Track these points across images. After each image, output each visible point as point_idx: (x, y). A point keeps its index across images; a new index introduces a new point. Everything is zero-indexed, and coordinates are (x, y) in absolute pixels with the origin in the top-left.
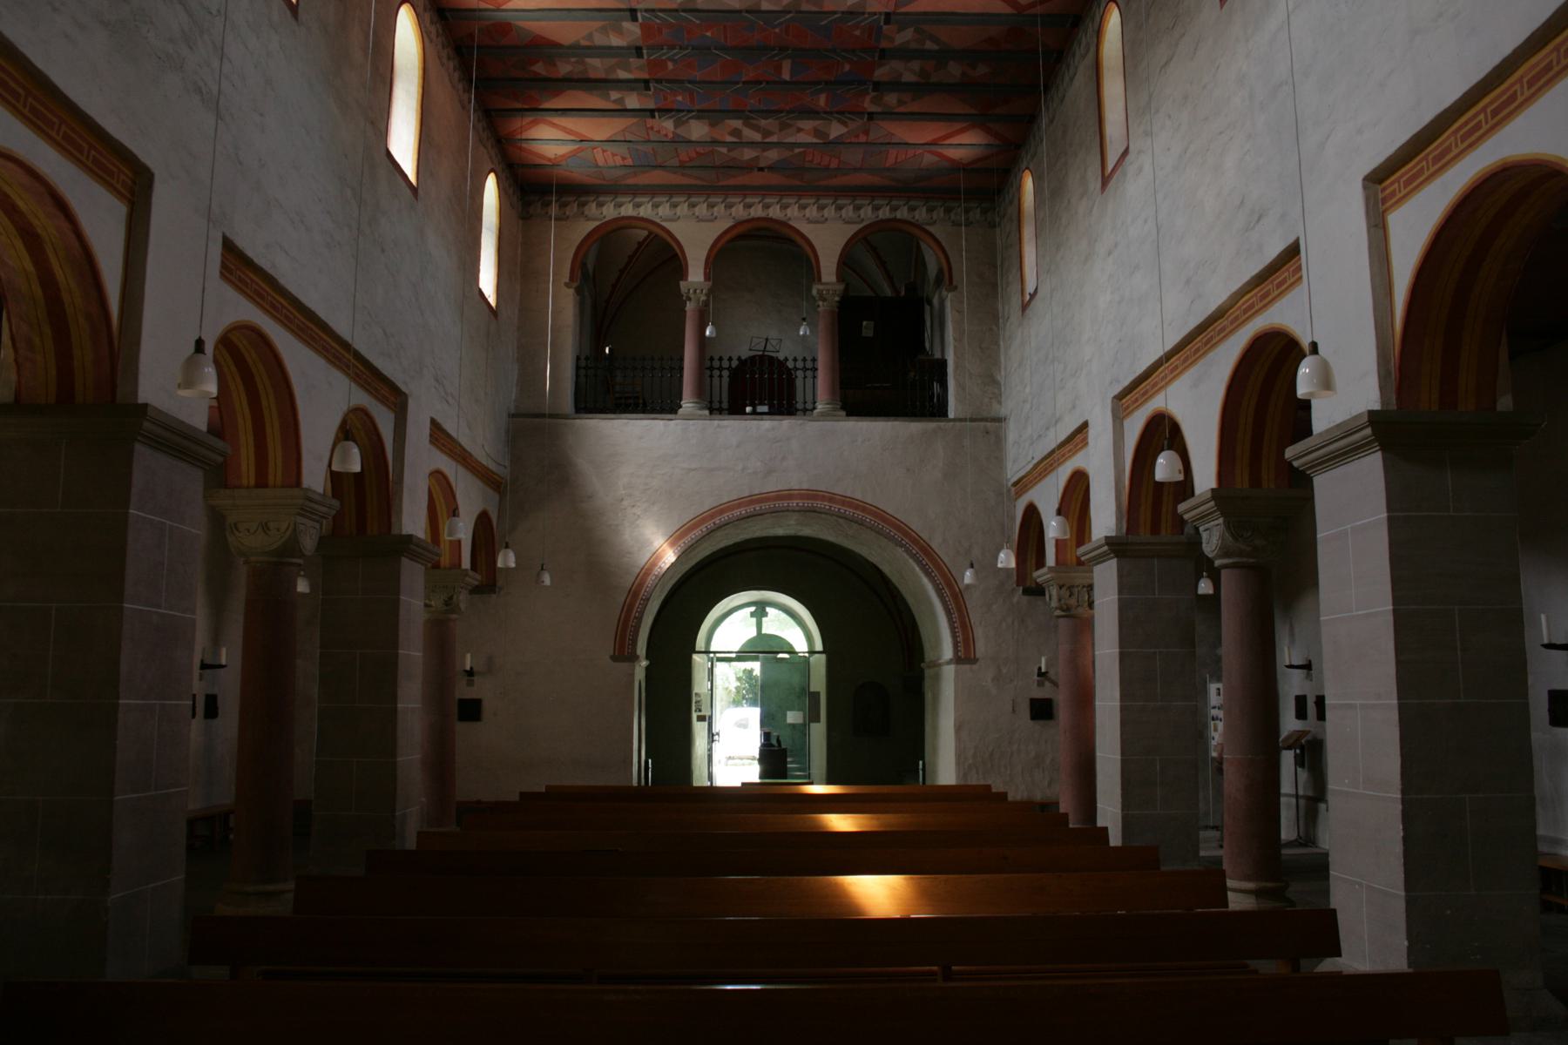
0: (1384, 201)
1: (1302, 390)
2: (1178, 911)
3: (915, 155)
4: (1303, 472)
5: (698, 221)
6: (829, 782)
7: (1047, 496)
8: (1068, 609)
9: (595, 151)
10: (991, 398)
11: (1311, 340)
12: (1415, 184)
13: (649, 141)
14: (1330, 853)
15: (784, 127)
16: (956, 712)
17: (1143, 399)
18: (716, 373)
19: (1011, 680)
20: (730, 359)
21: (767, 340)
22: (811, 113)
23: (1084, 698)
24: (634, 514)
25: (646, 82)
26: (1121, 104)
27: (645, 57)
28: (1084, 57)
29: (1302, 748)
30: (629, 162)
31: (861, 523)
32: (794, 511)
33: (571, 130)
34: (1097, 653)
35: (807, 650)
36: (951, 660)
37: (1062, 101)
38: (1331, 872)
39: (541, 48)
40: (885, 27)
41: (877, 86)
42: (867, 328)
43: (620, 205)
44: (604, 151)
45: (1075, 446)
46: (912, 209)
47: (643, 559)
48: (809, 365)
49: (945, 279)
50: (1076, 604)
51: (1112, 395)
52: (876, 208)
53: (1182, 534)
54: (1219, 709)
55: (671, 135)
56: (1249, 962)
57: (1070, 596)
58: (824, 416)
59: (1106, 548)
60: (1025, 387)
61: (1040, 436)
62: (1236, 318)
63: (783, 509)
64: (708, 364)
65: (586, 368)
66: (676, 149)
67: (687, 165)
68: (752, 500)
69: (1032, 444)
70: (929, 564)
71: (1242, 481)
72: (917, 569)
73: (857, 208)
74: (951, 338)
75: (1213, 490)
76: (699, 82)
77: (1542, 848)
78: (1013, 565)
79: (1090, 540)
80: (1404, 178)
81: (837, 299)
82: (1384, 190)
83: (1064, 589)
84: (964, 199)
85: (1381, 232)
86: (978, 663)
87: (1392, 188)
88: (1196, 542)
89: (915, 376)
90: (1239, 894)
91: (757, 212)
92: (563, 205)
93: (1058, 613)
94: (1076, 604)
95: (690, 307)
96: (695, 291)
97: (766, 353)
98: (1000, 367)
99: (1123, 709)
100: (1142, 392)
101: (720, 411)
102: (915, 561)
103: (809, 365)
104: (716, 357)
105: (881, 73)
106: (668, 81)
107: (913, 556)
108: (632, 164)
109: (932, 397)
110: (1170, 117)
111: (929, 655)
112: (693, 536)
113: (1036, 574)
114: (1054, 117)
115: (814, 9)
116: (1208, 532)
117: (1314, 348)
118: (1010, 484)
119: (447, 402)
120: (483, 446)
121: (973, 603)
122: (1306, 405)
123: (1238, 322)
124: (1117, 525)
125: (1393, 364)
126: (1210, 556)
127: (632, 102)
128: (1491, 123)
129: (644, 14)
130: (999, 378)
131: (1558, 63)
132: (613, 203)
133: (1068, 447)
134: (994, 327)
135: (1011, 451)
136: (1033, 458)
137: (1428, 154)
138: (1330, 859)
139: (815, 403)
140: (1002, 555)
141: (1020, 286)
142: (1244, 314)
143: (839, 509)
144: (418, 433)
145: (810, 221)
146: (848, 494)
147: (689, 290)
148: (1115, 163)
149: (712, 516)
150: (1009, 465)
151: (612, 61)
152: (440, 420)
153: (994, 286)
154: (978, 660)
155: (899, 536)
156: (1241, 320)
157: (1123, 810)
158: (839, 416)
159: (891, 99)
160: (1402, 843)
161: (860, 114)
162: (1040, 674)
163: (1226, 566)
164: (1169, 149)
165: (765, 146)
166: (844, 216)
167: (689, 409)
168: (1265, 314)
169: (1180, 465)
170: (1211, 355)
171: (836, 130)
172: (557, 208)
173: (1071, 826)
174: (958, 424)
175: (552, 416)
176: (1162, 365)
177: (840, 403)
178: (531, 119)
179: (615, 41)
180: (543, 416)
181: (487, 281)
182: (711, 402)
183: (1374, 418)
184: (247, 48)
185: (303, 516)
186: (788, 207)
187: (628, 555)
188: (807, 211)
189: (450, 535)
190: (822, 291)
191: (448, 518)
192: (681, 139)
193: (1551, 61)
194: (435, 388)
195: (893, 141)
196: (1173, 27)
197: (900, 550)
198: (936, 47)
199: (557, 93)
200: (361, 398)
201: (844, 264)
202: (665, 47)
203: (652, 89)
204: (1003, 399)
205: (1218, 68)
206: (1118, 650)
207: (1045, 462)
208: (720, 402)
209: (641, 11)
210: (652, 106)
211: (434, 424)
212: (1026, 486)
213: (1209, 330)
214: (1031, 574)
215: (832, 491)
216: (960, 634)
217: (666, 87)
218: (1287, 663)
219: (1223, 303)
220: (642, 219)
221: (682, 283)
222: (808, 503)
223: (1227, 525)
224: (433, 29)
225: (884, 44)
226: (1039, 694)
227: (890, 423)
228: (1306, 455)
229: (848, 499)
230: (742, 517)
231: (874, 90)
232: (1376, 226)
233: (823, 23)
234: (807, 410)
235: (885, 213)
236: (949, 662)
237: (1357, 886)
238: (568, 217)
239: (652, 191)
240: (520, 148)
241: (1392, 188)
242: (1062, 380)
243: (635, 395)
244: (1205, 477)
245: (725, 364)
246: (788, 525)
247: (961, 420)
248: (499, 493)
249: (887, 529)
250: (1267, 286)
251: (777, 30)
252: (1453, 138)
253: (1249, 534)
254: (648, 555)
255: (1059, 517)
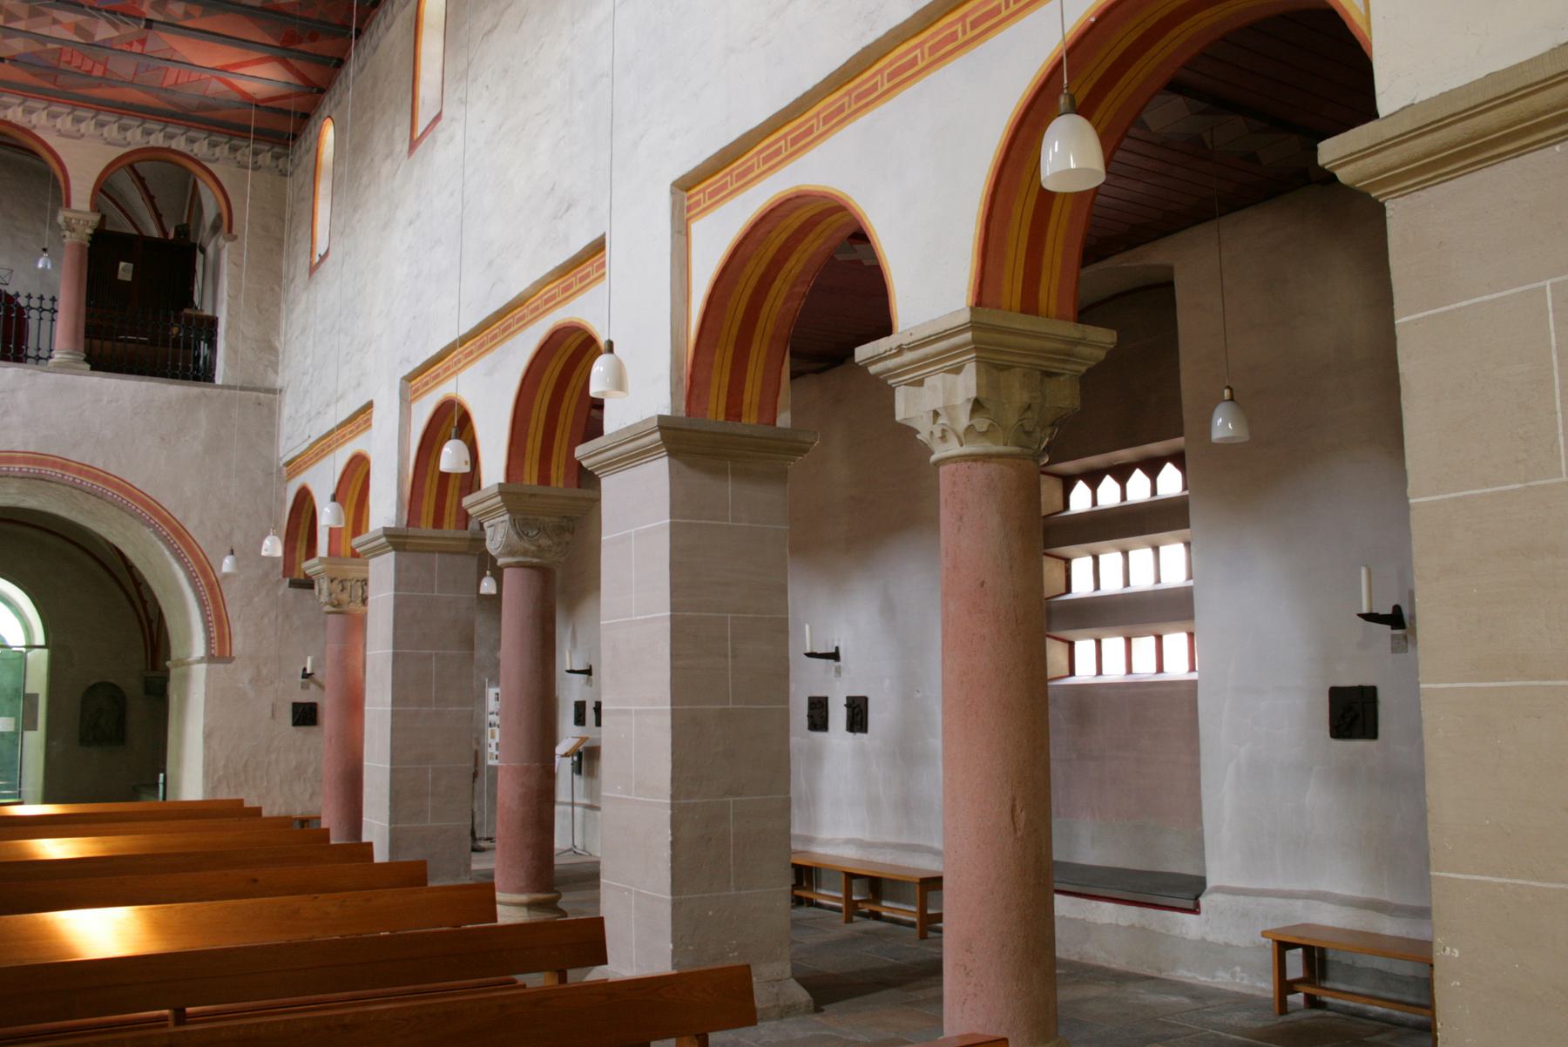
0: (689, 209)
1: (595, 390)
2: (445, 929)
3: (200, 80)
4: (591, 473)
5: (238, 167)
6: (47, 800)
7: (322, 480)
8: (339, 605)
10: (267, 366)
11: (607, 339)
12: (720, 196)
14: (602, 861)
16: (204, 718)
17: (434, 383)
19: (272, 682)
23: (353, 703)
26: (439, 65)
29: (580, 755)
34: (368, 653)
35: (24, 644)
36: (202, 658)
38: (602, 880)
42: (125, 271)
45: (358, 427)
48: (47, 304)
49: (224, 225)
50: (349, 599)
51: (401, 376)
53: (466, 529)
54: (497, 714)
56: (517, 977)
57: (342, 590)
58: (62, 368)
59: (384, 540)
60: (306, 358)
61: (319, 413)
62: (537, 308)
71: (530, 476)
72: (167, 553)
74: (225, 293)
75: (500, 484)
77: (795, 846)
78: (279, 552)
80: (709, 190)
81: (89, 231)
82: (689, 198)
83: (336, 582)
84: (254, 139)
85: (685, 238)
86: (234, 662)
87: (697, 198)
88: (479, 541)
89: (179, 332)
90: (512, 908)
93: (328, 608)
94: (349, 599)
98: (279, 332)
99: (394, 714)
100: (433, 375)
107: (164, 539)
111: (176, 652)
113: (305, 565)
116: (493, 528)
117: (610, 347)
118: (281, 463)
121: (231, 594)
122: (598, 405)
124: (397, 516)
125: (685, 371)
126: (493, 554)
128: (790, 150)
130: (277, 344)
131: (849, 107)
133: (350, 428)
134: (277, 288)
136: (309, 437)
137: (733, 170)
138: (601, 867)
140: (267, 542)
141: (309, 246)
142: (545, 304)
145: (60, 133)
153: (280, 242)
154: (234, 658)
155: (147, 514)
156: (541, 310)
157: (391, 823)
158: (83, 369)
160: (669, 847)
161: (137, 18)
162: (306, 676)
163: (509, 566)
164: (483, 122)
166: (106, 135)
169: (466, 456)
170: (508, 344)
171: (103, 31)
173: (333, 842)
174: (226, 392)
183: (666, 426)
188: (106, 130)
190: (71, 219)
193: (844, 104)
195: (174, 58)
197: (148, 531)
201: (102, 191)
205: (542, 46)
206: (391, 651)
212: (300, 466)
213: (508, 317)
214: (300, 564)
216: (214, 629)
218: (568, 669)
219: (524, 291)
222: (34, 469)
223: (513, 523)
226: (304, 697)
228: (595, 455)
229: (86, 468)
232: (679, 232)
234: (40, 358)
235: (157, 140)
236: (201, 661)
237: (626, 893)
241: (697, 198)
242: (348, 354)
244: (493, 471)
247: (229, 387)
249: (134, 505)
250: (571, 278)
252: (755, 159)
253: (535, 533)
255: (335, 504)
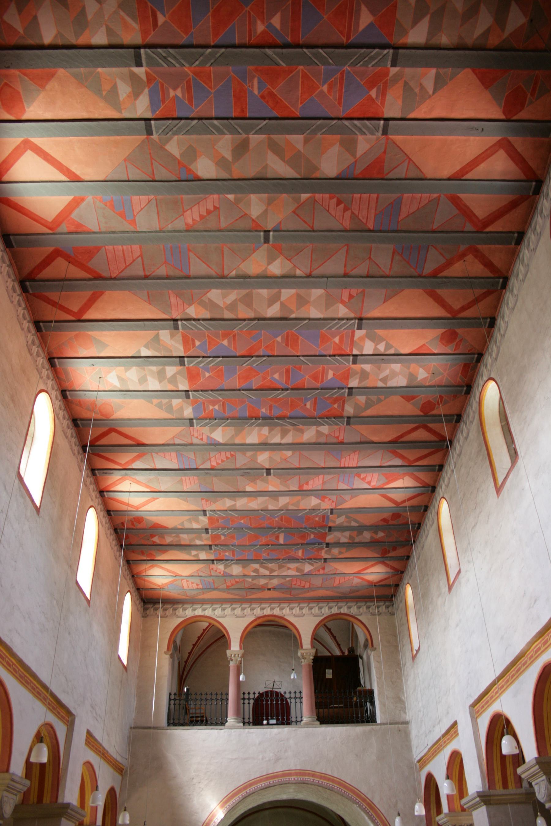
9: (183, 581)
13: (211, 576)
15: (281, 567)
18: (246, 701)
20: (254, 693)
21: (274, 682)
22: (295, 559)
24: (200, 787)
25: (210, 546)
27: (210, 533)
28: (432, 525)
30: (200, 587)
31: (331, 790)
32: (292, 783)
33: (171, 571)
37: (423, 548)
39: (157, 528)
40: (331, 516)
41: (328, 545)
42: (329, 674)
43: (194, 610)
44: (187, 581)
46: (349, 608)
47: (204, 817)
48: (298, 695)
49: (369, 644)
52: (330, 608)
53: (521, 787)
55: (222, 573)
58: (308, 725)
61: (430, 731)
62: (532, 656)
63: (286, 782)
64: (242, 696)
65: (175, 700)
66: (225, 580)
67: (230, 588)
68: (268, 777)
69: (426, 736)
70: (373, 814)
72: (367, 818)
73: (320, 608)
74: (375, 677)
75: (536, 758)
76: (238, 546)
78: (424, 813)
79: (467, 794)
88: (531, 794)
89: (357, 700)
91: (267, 612)
92: (165, 610)
95: (232, 664)
96: (235, 656)
97: (274, 690)
100: (485, 702)
101: (249, 723)
102: (365, 813)
103: (298, 695)
104: (246, 692)
105: (330, 538)
106: (221, 545)
108: (202, 588)
109: (367, 711)
110: (480, 552)
112: (234, 801)
113: (438, 818)
114: (419, 556)
115: (295, 508)
118: (416, 761)
119: (97, 720)
120: (115, 747)
123: (533, 658)
127: (203, 556)
129: (210, 512)
130: (403, 698)
132: (191, 608)
133: (448, 736)
135: (414, 742)
136: (427, 745)
139: (302, 717)
143: (319, 781)
144: (79, 737)
145: (295, 616)
146: (324, 772)
147: (231, 655)
148: (454, 578)
149: (245, 788)
150: (414, 749)
151: (193, 536)
152: (92, 730)
153: (396, 647)
159: (335, 551)
165: (271, 577)
167: (231, 723)
168: (548, 652)
170: (521, 678)
171: (308, 568)
172: (162, 612)
174: (383, 726)
175: (154, 728)
176: (496, 684)
177: (316, 717)
178: (150, 565)
179: (195, 526)
180: (150, 728)
181: (123, 651)
182: (244, 719)
184: (13, 528)
185: (7, 791)
186: (284, 609)
187: (196, 815)
189: (93, 802)
191: (92, 791)
192: (227, 575)
194: (91, 711)
196: (475, 508)
197: (355, 807)
198: (357, 525)
199: (165, 552)
200: (51, 718)
201: (315, 639)
202: (220, 528)
203: (213, 549)
204: (407, 711)
205: (501, 526)
207: (435, 746)
208: (249, 718)
209: (208, 511)
210: (212, 558)
211: (89, 734)
212: (425, 762)
214: (434, 818)
215: (314, 770)
217: (221, 548)
220: (207, 617)
221: (228, 651)
222: (300, 778)
224: (104, 520)
225: (330, 524)
227: (344, 727)
230: (262, 788)
231: (326, 547)
233: (300, 515)
235: (335, 610)
238: (167, 616)
239: (212, 602)
240: (144, 580)
242: (439, 697)
243: (202, 715)
245: (252, 696)
246: (289, 793)
247: (386, 724)
248: (122, 775)
249: (348, 792)
251: (277, 519)
254: (208, 814)
255: (448, 781)
